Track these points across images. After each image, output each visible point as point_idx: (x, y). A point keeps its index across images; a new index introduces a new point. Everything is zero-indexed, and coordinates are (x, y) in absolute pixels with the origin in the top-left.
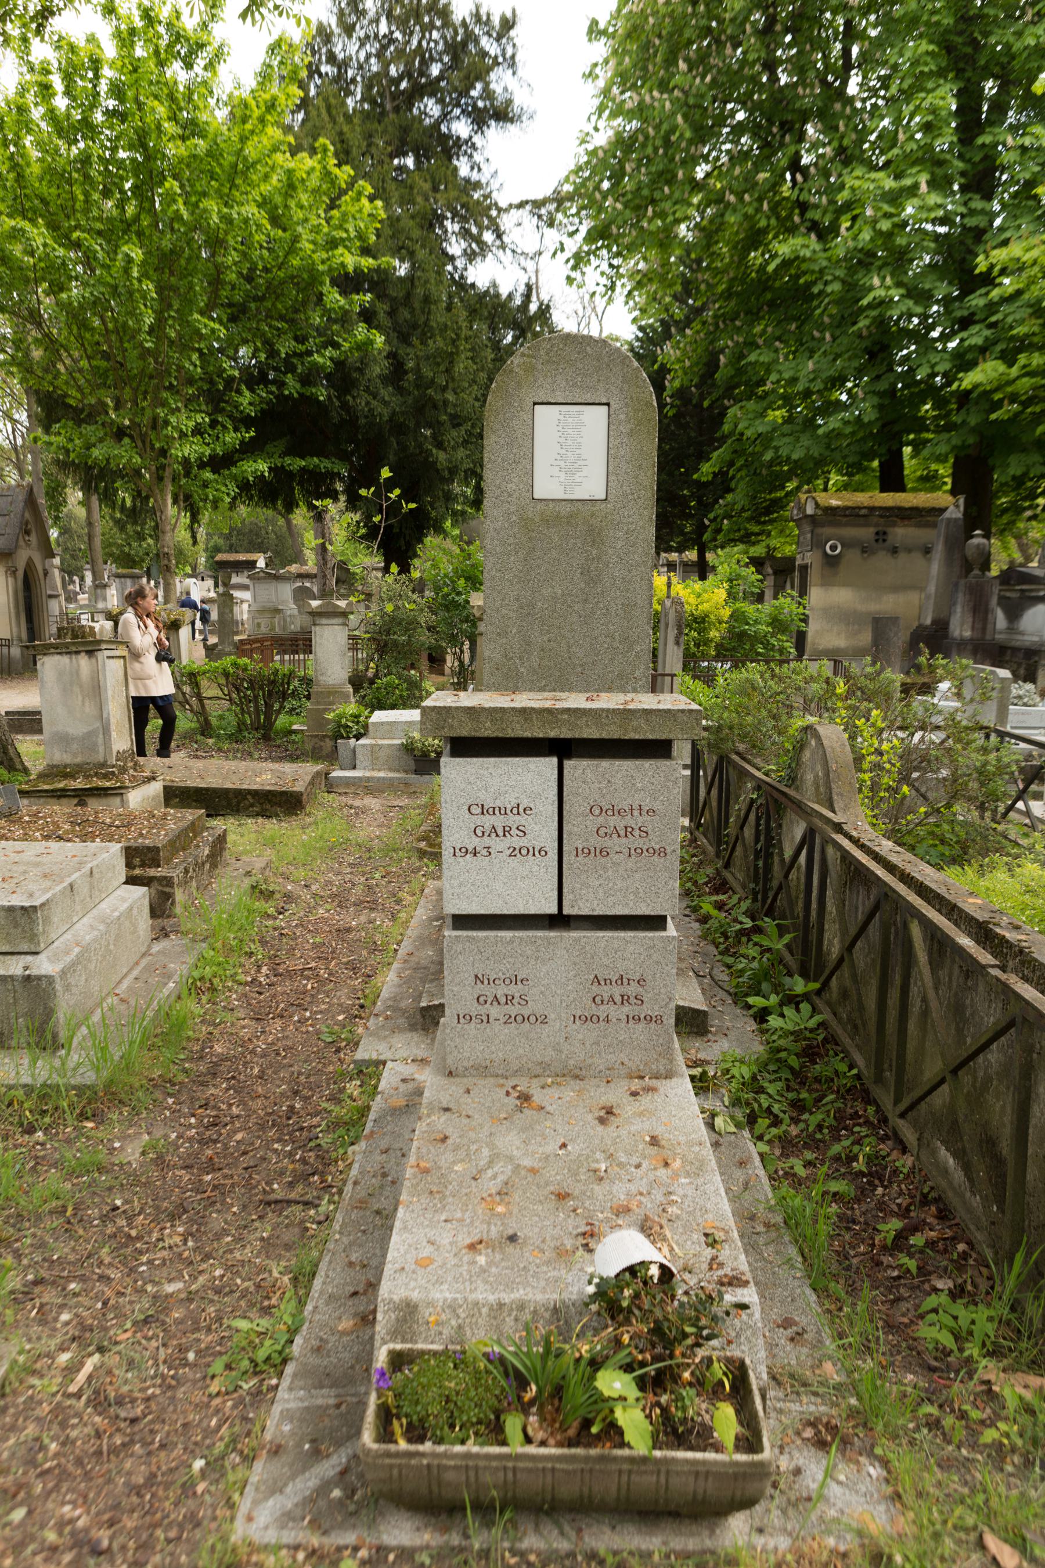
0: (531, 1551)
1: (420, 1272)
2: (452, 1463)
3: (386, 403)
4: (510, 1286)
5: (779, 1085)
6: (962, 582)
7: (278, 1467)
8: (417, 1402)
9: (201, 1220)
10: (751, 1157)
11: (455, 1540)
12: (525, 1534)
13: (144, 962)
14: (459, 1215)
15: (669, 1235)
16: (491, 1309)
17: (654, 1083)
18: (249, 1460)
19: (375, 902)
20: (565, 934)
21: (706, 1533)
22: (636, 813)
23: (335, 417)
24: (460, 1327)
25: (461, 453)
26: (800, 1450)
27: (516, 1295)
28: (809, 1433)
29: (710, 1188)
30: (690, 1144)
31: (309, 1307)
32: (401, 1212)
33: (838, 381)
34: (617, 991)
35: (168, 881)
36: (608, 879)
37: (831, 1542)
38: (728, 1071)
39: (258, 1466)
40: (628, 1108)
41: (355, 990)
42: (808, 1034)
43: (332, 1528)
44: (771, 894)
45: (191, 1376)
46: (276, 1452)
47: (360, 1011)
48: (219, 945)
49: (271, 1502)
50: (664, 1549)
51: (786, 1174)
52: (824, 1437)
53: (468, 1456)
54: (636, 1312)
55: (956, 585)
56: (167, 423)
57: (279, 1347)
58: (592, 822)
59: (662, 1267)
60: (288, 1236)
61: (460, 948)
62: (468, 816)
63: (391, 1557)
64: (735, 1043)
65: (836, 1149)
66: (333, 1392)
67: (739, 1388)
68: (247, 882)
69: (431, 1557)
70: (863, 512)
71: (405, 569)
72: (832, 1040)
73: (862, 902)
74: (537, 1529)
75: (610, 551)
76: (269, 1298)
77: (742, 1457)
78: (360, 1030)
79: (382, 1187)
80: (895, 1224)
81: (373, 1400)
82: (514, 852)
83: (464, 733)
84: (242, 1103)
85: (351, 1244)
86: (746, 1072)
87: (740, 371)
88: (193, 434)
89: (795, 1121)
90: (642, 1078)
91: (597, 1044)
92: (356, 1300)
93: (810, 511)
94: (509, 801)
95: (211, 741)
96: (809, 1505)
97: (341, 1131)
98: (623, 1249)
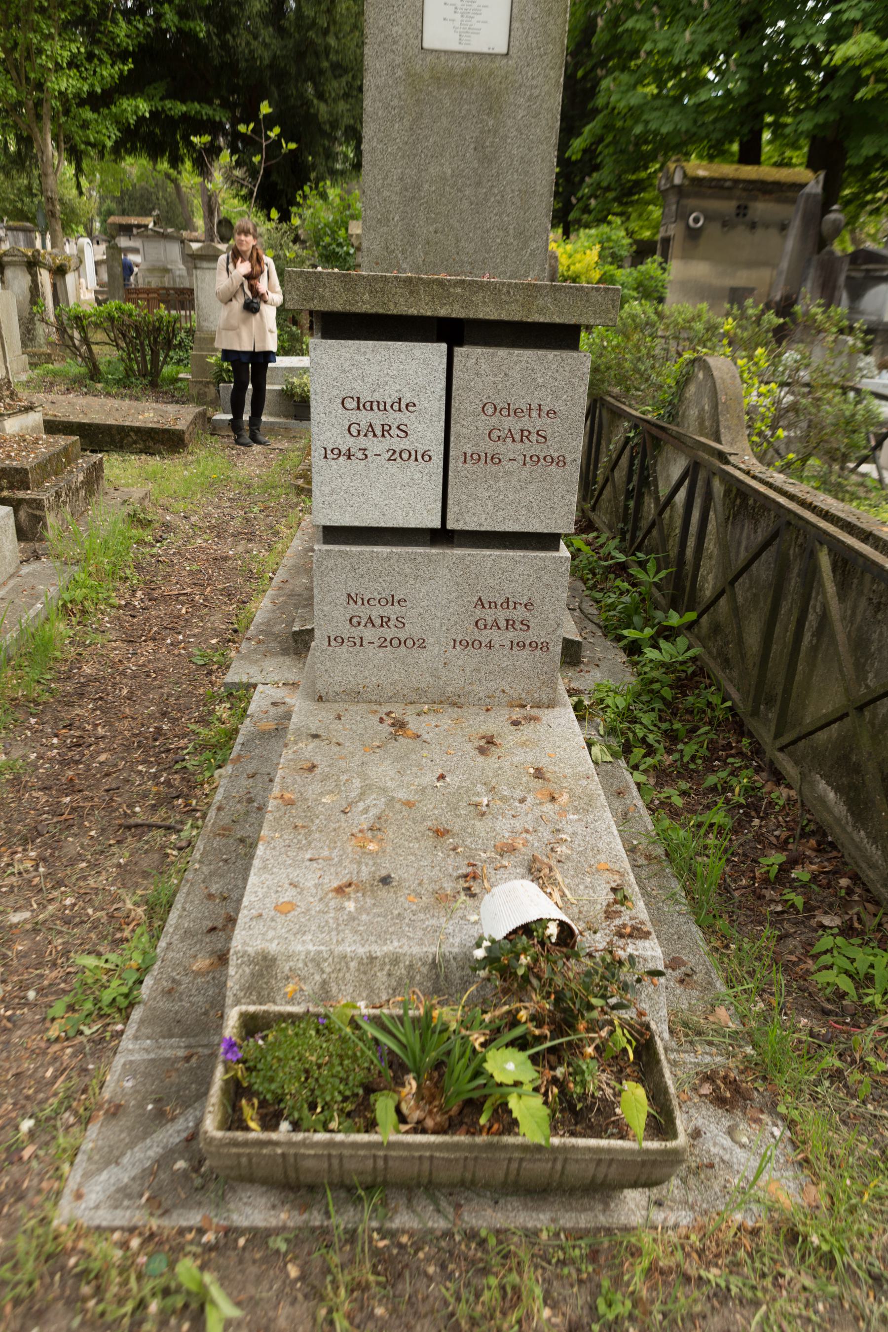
0: (404, 1232)
1: (281, 919)
2: (312, 1152)
3: (266, 46)
4: (382, 937)
5: (653, 716)
6: (815, 258)
7: (117, 1132)
8: (271, 1080)
9: (56, 844)
10: (628, 787)
11: (316, 1219)
12: (395, 1211)
13: (12, 583)
14: (326, 853)
15: (559, 878)
16: (361, 963)
17: (535, 712)
18: (85, 1121)
19: (253, 534)
20: (448, 551)
21: (600, 1207)
22: (534, 414)
23: (216, 57)
24: (324, 982)
25: (342, 106)
26: (698, 1109)
27: (389, 948)
28: (706, 1089)
29: (601, 826)
30: (577, 777)
31: (162, 944)
32: (260, 850)
33: (708, 57)
34: (502, 616)
35: (37, 504)
36: (498, 490)
37: (738, 1217)
38: (602, 700)
39: (93, 1130)
40: (509, 738)
41: (229, 615)
42: (680, 668)
43: (175, 1206)
44: (640, 534)
45: (29, 1017)
46: (114, 1115)
47: (233, 635)
48: (92, 569)
49: (104, 1176)
50: (552, 1227)
51: (661, 803)
52: (728, 1095)
53: (331, 1144)
54: (535, 982)
55: (809, 261)
56: (40, 51)
57: (125, 990)
58: (484, 423)
59: (562, 924)
60: (146, 862)
61: (330, 563)
62: (341, 410)
63: (242, 1242)
64: (608, 673)
65: (712, 780)
66: (183, 1042)
67: (644, 1061)
68: (127, 509)
69: (287, 1241)
70: (728, 184)
71: (285, 217)
72: (701, 672)
73: (750, 536)
74: (409, 1206)
75: (510, 122)
76: (121, 930)
77: (654, 1145)
78: (233, 654)
79: (247, 813)
80: (776, 858)
81: (219, 1075)
82: (394, 455)
83: (338, 306)
84: (108, 724)
85: (212, 874)
86: (621, 703)
87: (616, 38)
88: (70, 65)
89: (669, 752)
90: (523, 706)
91: (479, 671)
92: (213, 937)
93: (677, 180)
94: (389, 395)
95: (100, 386)
96: (710, 1172)
97: (207, 754)
98: (515, 904)
